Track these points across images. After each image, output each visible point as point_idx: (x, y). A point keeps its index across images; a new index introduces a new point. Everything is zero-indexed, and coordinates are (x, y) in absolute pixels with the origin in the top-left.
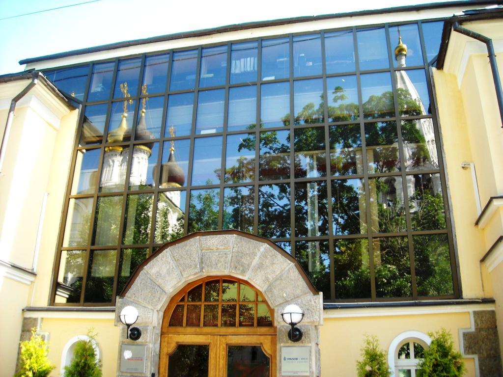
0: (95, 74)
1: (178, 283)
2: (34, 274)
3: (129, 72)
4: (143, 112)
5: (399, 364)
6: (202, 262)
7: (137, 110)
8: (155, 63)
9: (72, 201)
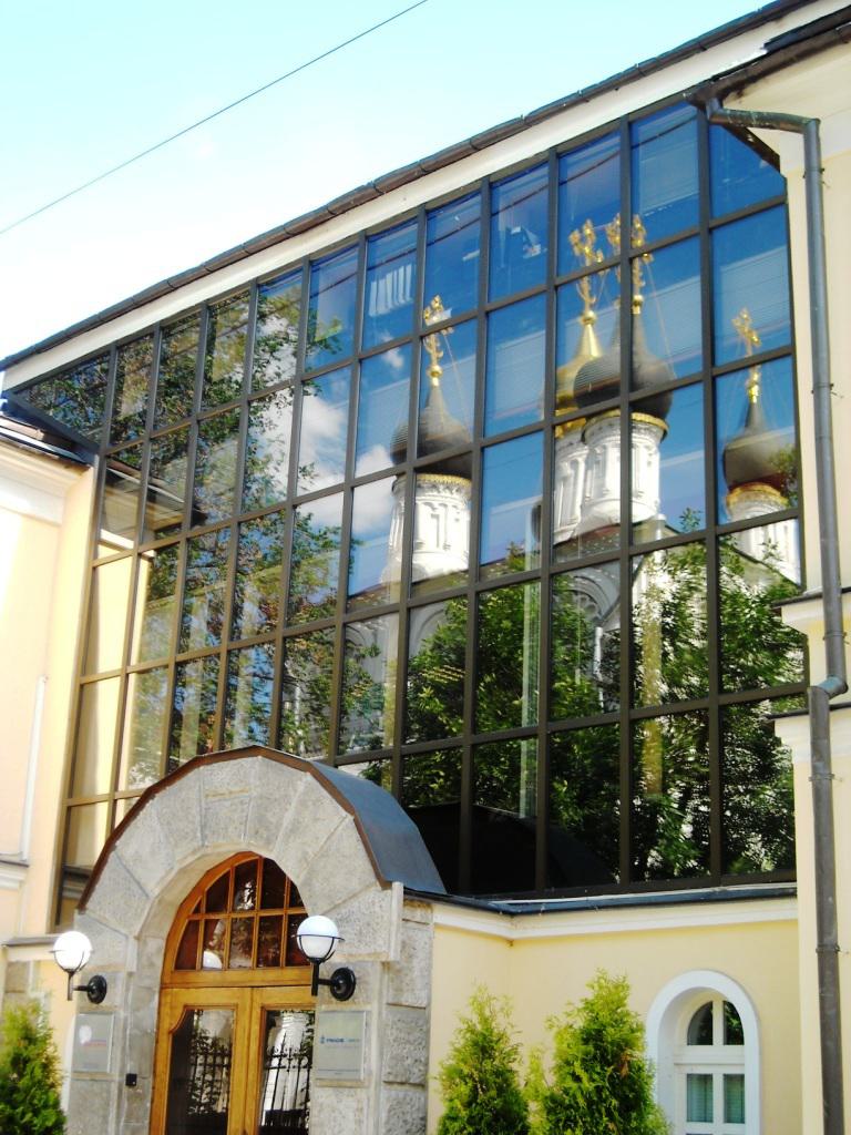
0: (501, 215)
1: (168, 873)
2: (23, 865)
3: (595, 178)
4: (433, 374)
5: (685, 1060)
6: (203, 827)
7: (417, 369)
8: (580, 171)
9: (133, 677)
